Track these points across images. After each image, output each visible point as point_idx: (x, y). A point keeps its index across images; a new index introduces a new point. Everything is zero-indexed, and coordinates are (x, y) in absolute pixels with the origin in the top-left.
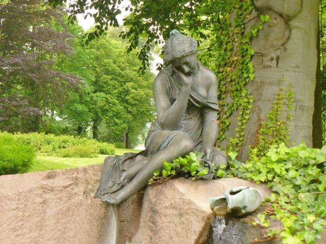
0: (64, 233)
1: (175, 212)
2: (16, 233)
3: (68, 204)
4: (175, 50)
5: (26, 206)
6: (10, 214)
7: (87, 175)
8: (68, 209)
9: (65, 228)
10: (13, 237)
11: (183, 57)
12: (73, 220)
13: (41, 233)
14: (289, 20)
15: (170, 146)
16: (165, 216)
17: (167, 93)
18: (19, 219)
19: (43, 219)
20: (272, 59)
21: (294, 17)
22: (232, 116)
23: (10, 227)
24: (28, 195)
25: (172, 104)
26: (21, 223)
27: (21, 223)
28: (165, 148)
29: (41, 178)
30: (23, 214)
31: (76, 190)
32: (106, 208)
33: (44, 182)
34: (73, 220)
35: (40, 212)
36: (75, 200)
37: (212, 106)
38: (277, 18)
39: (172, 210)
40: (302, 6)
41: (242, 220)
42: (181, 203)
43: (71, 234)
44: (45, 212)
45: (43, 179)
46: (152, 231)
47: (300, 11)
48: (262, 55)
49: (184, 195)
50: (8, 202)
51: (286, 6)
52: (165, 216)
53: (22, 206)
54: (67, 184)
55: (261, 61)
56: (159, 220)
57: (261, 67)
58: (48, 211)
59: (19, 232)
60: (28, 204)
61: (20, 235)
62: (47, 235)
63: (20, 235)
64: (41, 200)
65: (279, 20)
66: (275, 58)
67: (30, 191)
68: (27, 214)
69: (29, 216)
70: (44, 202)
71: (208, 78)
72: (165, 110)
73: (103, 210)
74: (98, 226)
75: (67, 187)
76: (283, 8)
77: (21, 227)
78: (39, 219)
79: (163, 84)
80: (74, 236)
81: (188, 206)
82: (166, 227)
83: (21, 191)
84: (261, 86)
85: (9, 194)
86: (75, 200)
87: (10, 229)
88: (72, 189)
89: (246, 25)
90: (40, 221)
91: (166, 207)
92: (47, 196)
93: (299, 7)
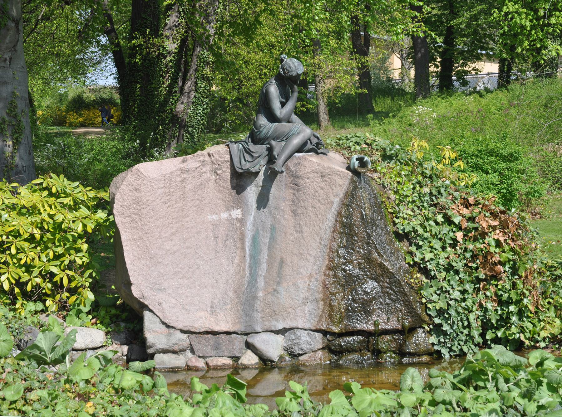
0: (201, 201)
2: (167, 205)
3: (200, 180)
5: (170, 184)
6: (160, 191)
8: (201, 183)
9: (202, 197)
19: (184, 193)
23: (162, 201)
29: (178, 163)
31: (204, 169)
33: (181, 166)
36: (205, 176)
42: (320, 168)
43: (207, 201)
44: (185, 187)
50: (156, 182)
54: (198, 166)
56: (301, 182)
64: (180, 179)
67: (172, 173)
68: (172, 190)
69: (173, 192)
70: (183, 180)
77: (169, 200)
78: (181, 193)
80: (209, 203)
92: (185, 176)
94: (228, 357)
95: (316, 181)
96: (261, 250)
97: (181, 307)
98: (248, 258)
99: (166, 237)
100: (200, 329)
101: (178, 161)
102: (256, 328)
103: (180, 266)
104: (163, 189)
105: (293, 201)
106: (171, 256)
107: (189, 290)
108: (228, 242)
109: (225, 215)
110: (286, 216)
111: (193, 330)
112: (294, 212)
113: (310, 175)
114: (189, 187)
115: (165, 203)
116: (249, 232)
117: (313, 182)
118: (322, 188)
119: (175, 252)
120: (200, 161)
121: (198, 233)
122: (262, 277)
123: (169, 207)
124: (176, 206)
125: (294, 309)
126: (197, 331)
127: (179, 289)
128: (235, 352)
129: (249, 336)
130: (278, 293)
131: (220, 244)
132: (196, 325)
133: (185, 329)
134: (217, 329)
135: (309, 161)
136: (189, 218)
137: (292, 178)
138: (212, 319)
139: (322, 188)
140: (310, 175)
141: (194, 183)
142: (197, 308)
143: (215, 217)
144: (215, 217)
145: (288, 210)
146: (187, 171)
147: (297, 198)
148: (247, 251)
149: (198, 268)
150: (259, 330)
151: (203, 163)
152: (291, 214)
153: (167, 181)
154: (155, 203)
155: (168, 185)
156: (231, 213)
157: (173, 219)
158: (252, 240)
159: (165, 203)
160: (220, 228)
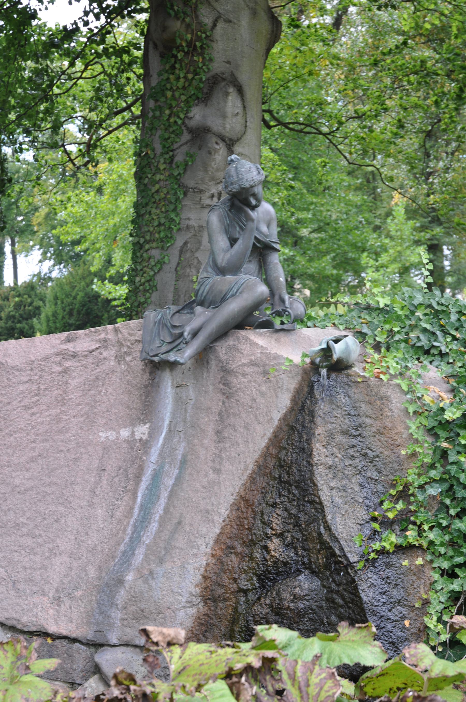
0: (94, 407)
1: (256, 369)
2: (30, 411)
3: (95, 372)
4: (242, 179)
5: (41, 377)
6: (22, 388)
7: (120, 336)
8: (97, 378)
9: (95, 401)
10: (27, 416)
11: (252, 187)
12: (104, 391)
13: (63, 409)
14: (233, 144)
15: (240, 293)
16: (244, 375)
17: (226, 230)
18: (33, 394)
19: (65, 392)
20: (212, 196)
21: (238, 140)
22: (161, 272)
23: (23, 404)
24: (43, 363)
25: (232, 246)
26: (37, 398)
27: (37, 398)
28: (233, 295)
29: (58, 342)
30: (39, 387)
31: (105, 354)
32: (151, 373)
33: (64, 347)
34: (104, 391)
35: (60, 383)
36: (106, 366)
37: (274, 245)
38: (219, 142)
39: (252, 367)
40: (246, 126)
41: (346, 372)
42: (264, 358)
43: (103, 407)
44: (66, 383)
45: (61, 343)
46: (224, 394)
47: (244, 133)
48: (201, 191)
49: (266, 349)
50: (17, 373)
51: (228, 126)
52: (244, 375)
53: (36, 377)
54: (93, 347)
55: (198, 199)
56: (234, 381)
57: (198, 206)
58: (70, 381)
59: (35, 410)
60: (44, 374)
61: (37, 413)
62: (71, 411)
63: (37, 413)
64: (60, 369)
65: (221, 145)
66: (216, 194)
67: (45, 359)
68: (43, 387)
69: (46, 390)
70: (65, 371)
71: (268, 213)
72: (226, 251)
73: (146, 376)
74: (141, 395)
75: (93, 351)
76: (225, 128)
77: (36, 404)
78: (59, 392)
79: (220, 221)
80: (107, 410)
81: (276, 362)
82: (245, 387)
83: (33, 359)
84: (200, 231)
85: (18, 363)
86: (106, 366)
87: (23, 406)
88: (100, 353)
89: (176, 152)
90: (61, 395)
91: (244, 365)
92: (69, 364)
93: (243, 129)
94: (64, 682)
95: (255, 381)
96: (159, 497)
97: (11, 583)
98: (136, 511)
99: (19, 463)
100: (29, 627)
101: (59, 338)
102: (109, 637)
103: (28, 515)
104: (28, 385)
105: (220, 415)
106: (18, 496)
107: (32, 557)
108: (116, 480)
109: (125, 433)
110: (205, 442)
111: (19, 627)
112: (218, 433)
113: (247, 370)
114: (73, 383)
115: (27, 408)
116: (151, 465)
117: (250, 381)
118: (262, 394)
119: (26, 490)
120: (100, 341)
121: (75, 460)
122: (144, 547)
123: (33, 414)
124: (47, 414)
125: (173, 612)
126: (26, 629)
127: (15, 554)
128: (74, 675)
129: (100, 650)
130: (153, 579)
131: (105, 482)
132: (25, 619)
133: (9, 623)
134: (52, 629)
135: (253, 344)
136: (68, 435)
137: (222, 374)
138: (51, 611)
139: (262, 394)
140: (247, 370)
141: (85, 376)
142: (35, 589)
143: (112, 435)
144: (112, 435)
145: (210, 430)
146: (74, 356)
147: (226, 411)
148: (139, 499)
149: (57, 521)
150: (114, 641)
151: (105, 343)
152: (214, 438)
153: (36, 371)
154: (9, 407)
155: (36, 377)
156: (136, 429)
157: (37, 435)
158: (152, 479)
159: (27, 408)
160: (113, 455)
